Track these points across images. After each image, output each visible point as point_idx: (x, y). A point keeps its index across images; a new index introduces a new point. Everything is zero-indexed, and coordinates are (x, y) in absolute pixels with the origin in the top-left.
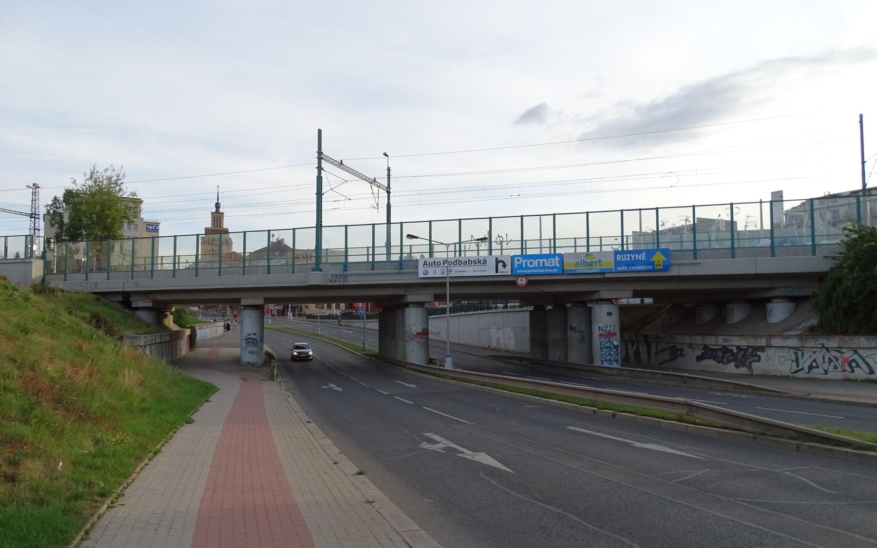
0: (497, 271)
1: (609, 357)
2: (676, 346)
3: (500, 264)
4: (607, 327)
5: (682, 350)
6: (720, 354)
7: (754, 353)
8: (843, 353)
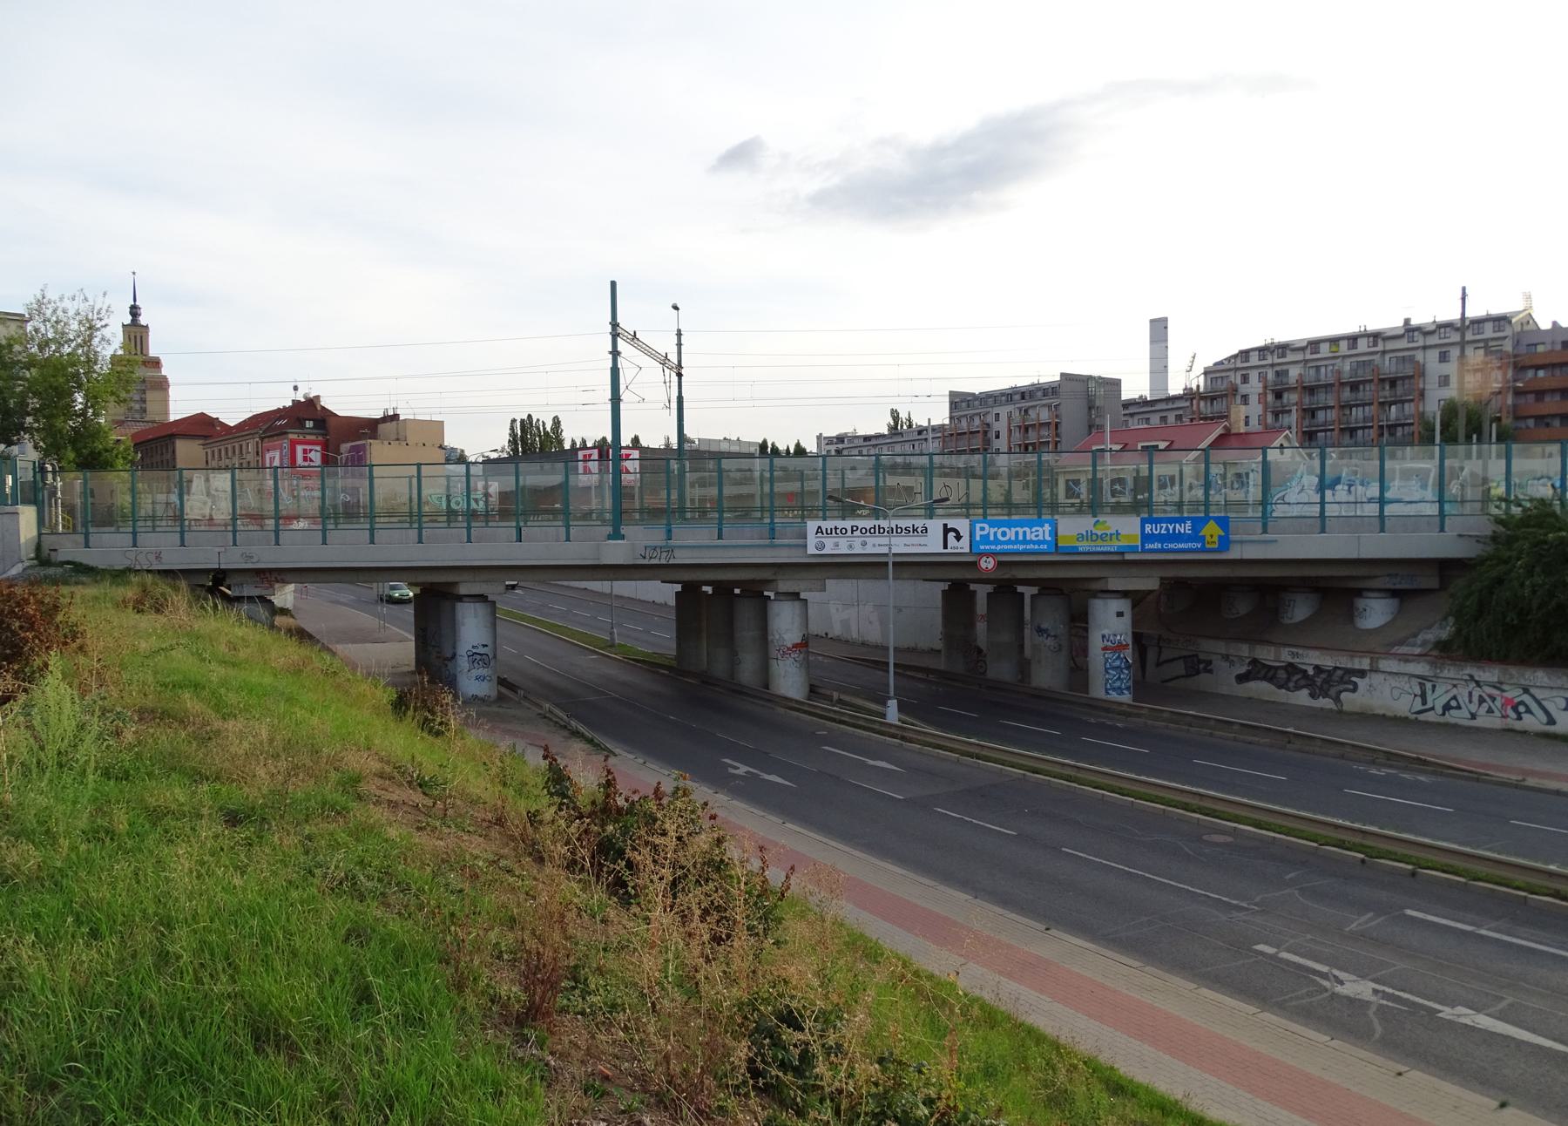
0: (945, 547)
1: (1118, 684)
2: (1197, 656)
3: (951, 535)
4: (1115, 635)
5: (1210, 662)
6: (1282, 675)
7: (1346, 678)
8: (1503, 691)
